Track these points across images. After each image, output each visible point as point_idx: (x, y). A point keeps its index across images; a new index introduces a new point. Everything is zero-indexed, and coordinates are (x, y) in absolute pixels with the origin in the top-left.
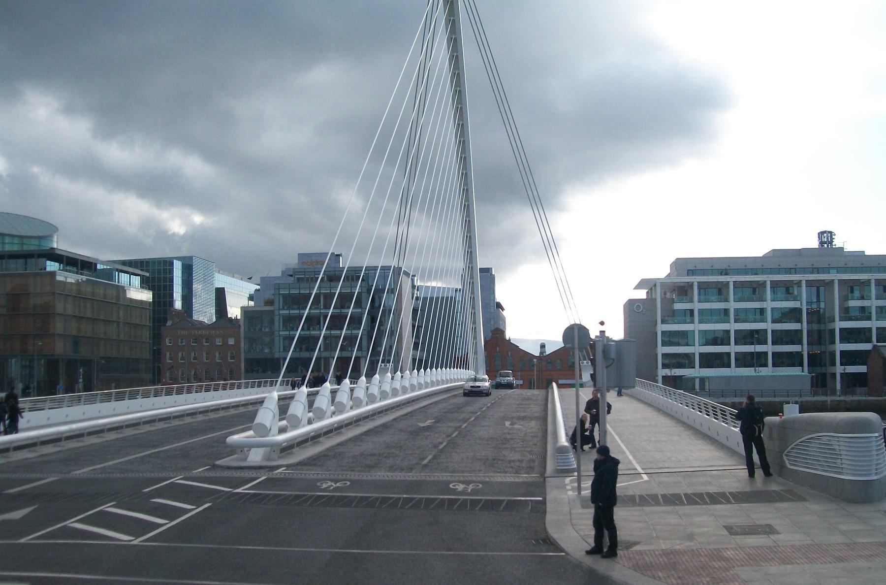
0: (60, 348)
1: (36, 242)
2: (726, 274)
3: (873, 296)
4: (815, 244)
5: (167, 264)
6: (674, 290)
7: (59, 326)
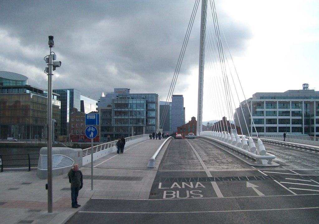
0: (31, 122)
1: (21, 83)
2: (275, 99)
3: (278, 107)
4: (302, 89)
7: (31, 113)
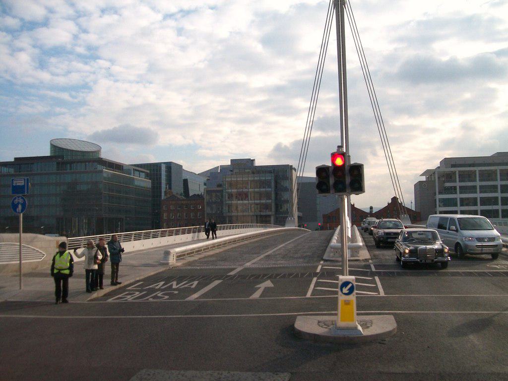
2: (474, 166)
6: (443, 176)
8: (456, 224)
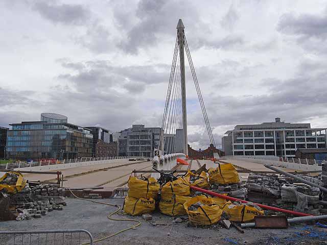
5: (97, 129)
8: (188, 149)
